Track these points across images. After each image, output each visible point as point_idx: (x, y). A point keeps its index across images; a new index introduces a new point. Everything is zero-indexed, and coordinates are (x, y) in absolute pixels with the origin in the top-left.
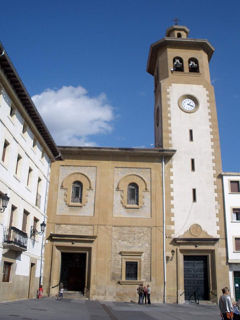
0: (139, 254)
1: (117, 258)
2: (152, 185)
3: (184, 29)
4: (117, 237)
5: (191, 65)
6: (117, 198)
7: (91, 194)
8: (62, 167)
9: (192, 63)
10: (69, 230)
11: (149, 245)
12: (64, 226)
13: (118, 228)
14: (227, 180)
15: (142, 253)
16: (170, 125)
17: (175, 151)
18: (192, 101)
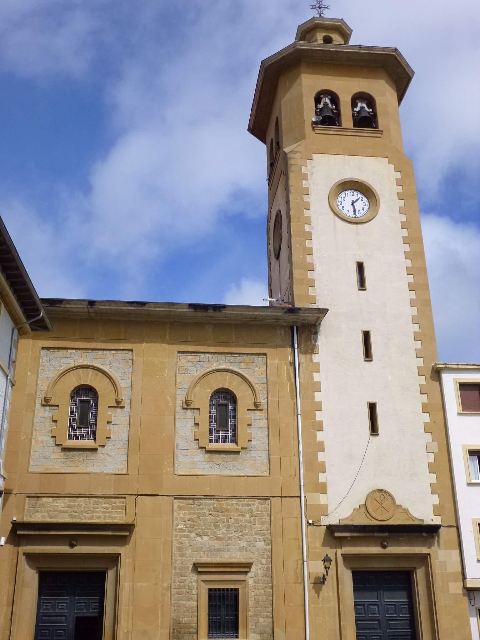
0: (244, 568)
1: (185, 580)
2: (270, 394)
3: (340, 25)
4: (186, 526)
5: (357, 109)
6: (185, 427)
7: (120, 418)
8: (45, 352)
9: (359, 105)
10: (60, 511)
11: (267, 545)
12: (50, 500)
13: (188, 501)
14: (450, 381)
15: (249, 565)
16: (309, 251)
17: (324, 311)
18: (360, 195)
